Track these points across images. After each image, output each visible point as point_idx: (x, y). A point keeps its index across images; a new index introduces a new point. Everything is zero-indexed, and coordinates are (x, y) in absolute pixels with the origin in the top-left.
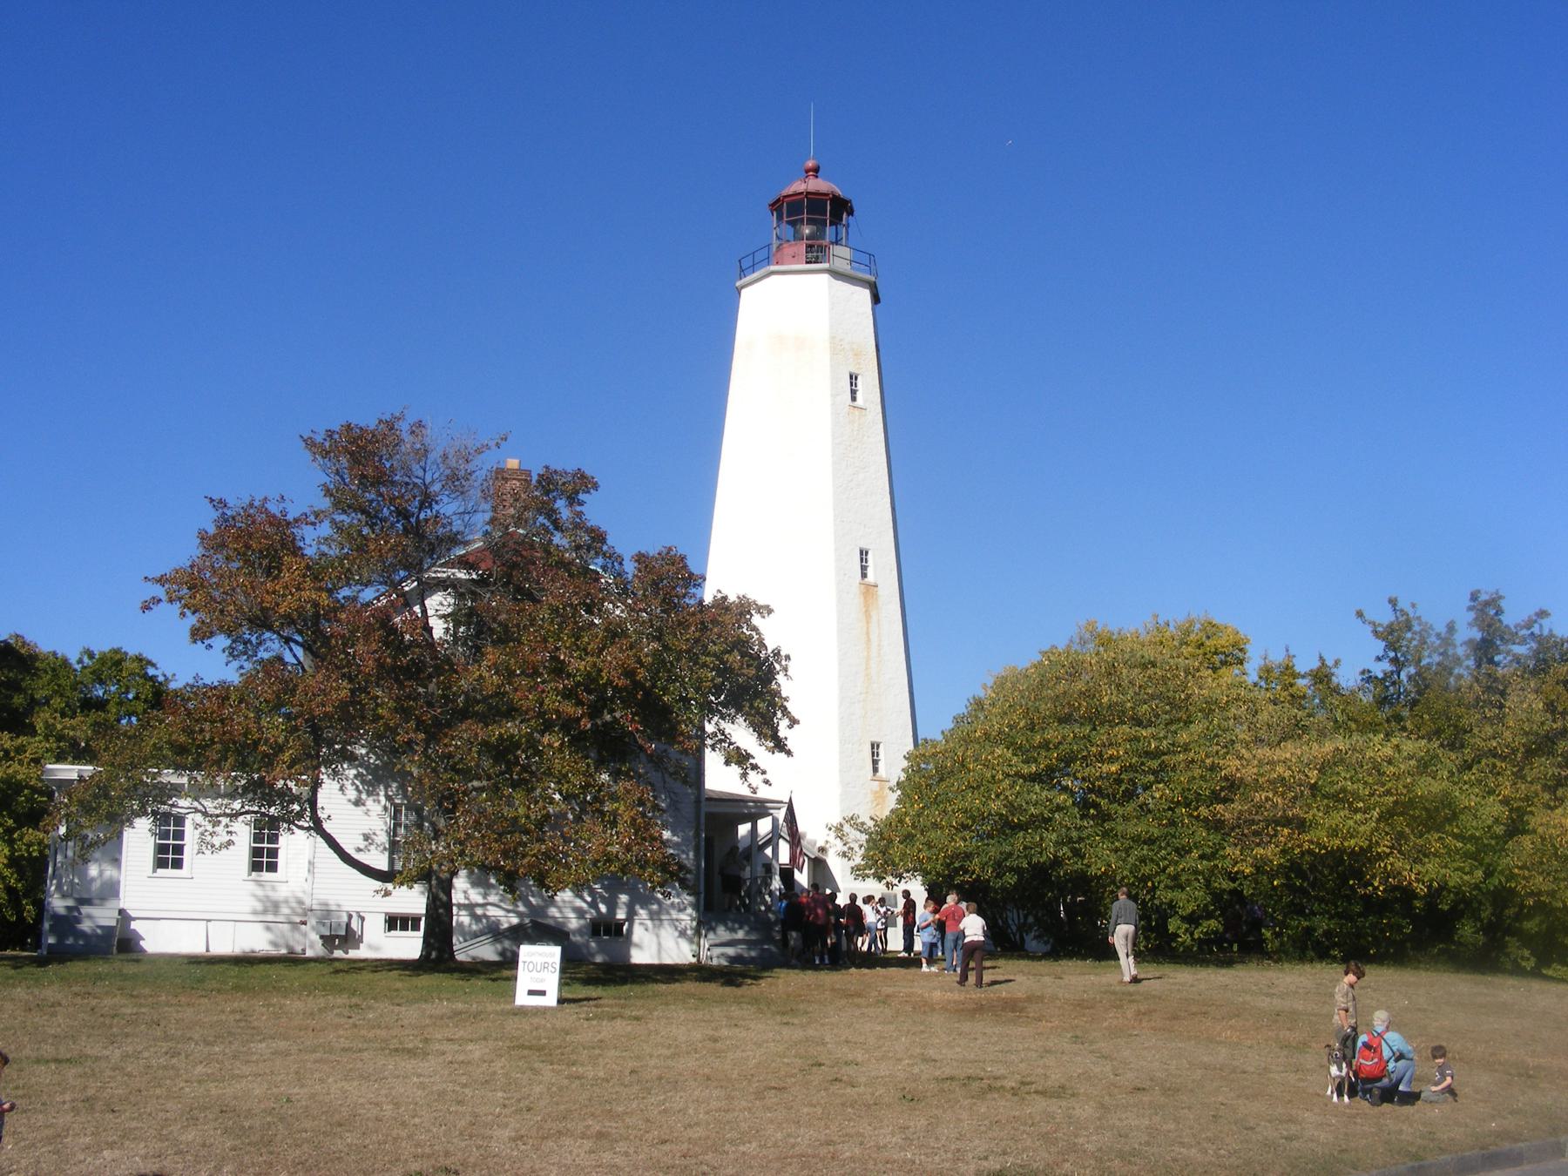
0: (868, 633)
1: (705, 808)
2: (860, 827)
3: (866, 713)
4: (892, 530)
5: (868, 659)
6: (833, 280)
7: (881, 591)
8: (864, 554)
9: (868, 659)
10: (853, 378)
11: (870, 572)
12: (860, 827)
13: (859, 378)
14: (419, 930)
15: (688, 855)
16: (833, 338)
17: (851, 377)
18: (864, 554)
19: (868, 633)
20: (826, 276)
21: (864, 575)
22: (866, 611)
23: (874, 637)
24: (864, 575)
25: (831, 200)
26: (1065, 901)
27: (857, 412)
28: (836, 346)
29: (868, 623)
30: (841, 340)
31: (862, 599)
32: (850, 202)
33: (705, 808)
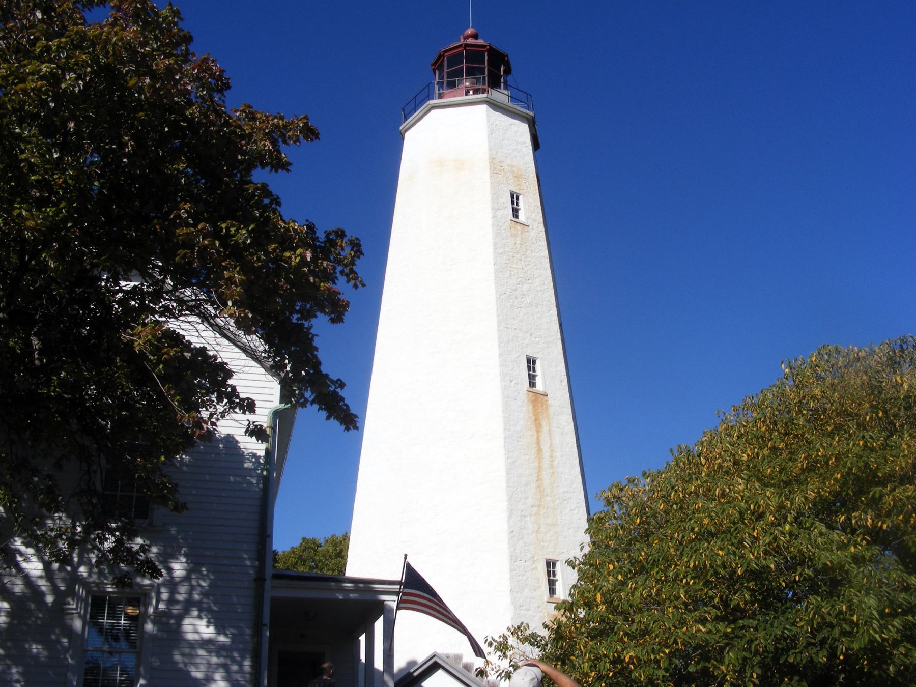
0: (538, 443)
1: (272, 591)
2: (533, 640)
3: (539, 528)
4: (560, 342)
5: (540, 468)
6: (491, 111)
7: (551, 400)
8: (531, 363)
9: (540, 468)
10: (515, 198)
11: (539, 381)
12: (533, 640)
13: (521, 198)
14: (273, 599)
15: (241, 665)
16: (492, 159)
17: (512, 196)
18: (531, 363)
19: (538, 443)
20: (484, 107)
21: (532, 384)
22: (536, 420)
23: (545, 448)
24: (532, 384)
25: (488, 51)
26: (153, 260)
27: (519, 227)
28: (496, 168)
29: (538, 432)
30: (501, 162)
31: (531, 407)
32: (507, 56)
33: (272, 591)
